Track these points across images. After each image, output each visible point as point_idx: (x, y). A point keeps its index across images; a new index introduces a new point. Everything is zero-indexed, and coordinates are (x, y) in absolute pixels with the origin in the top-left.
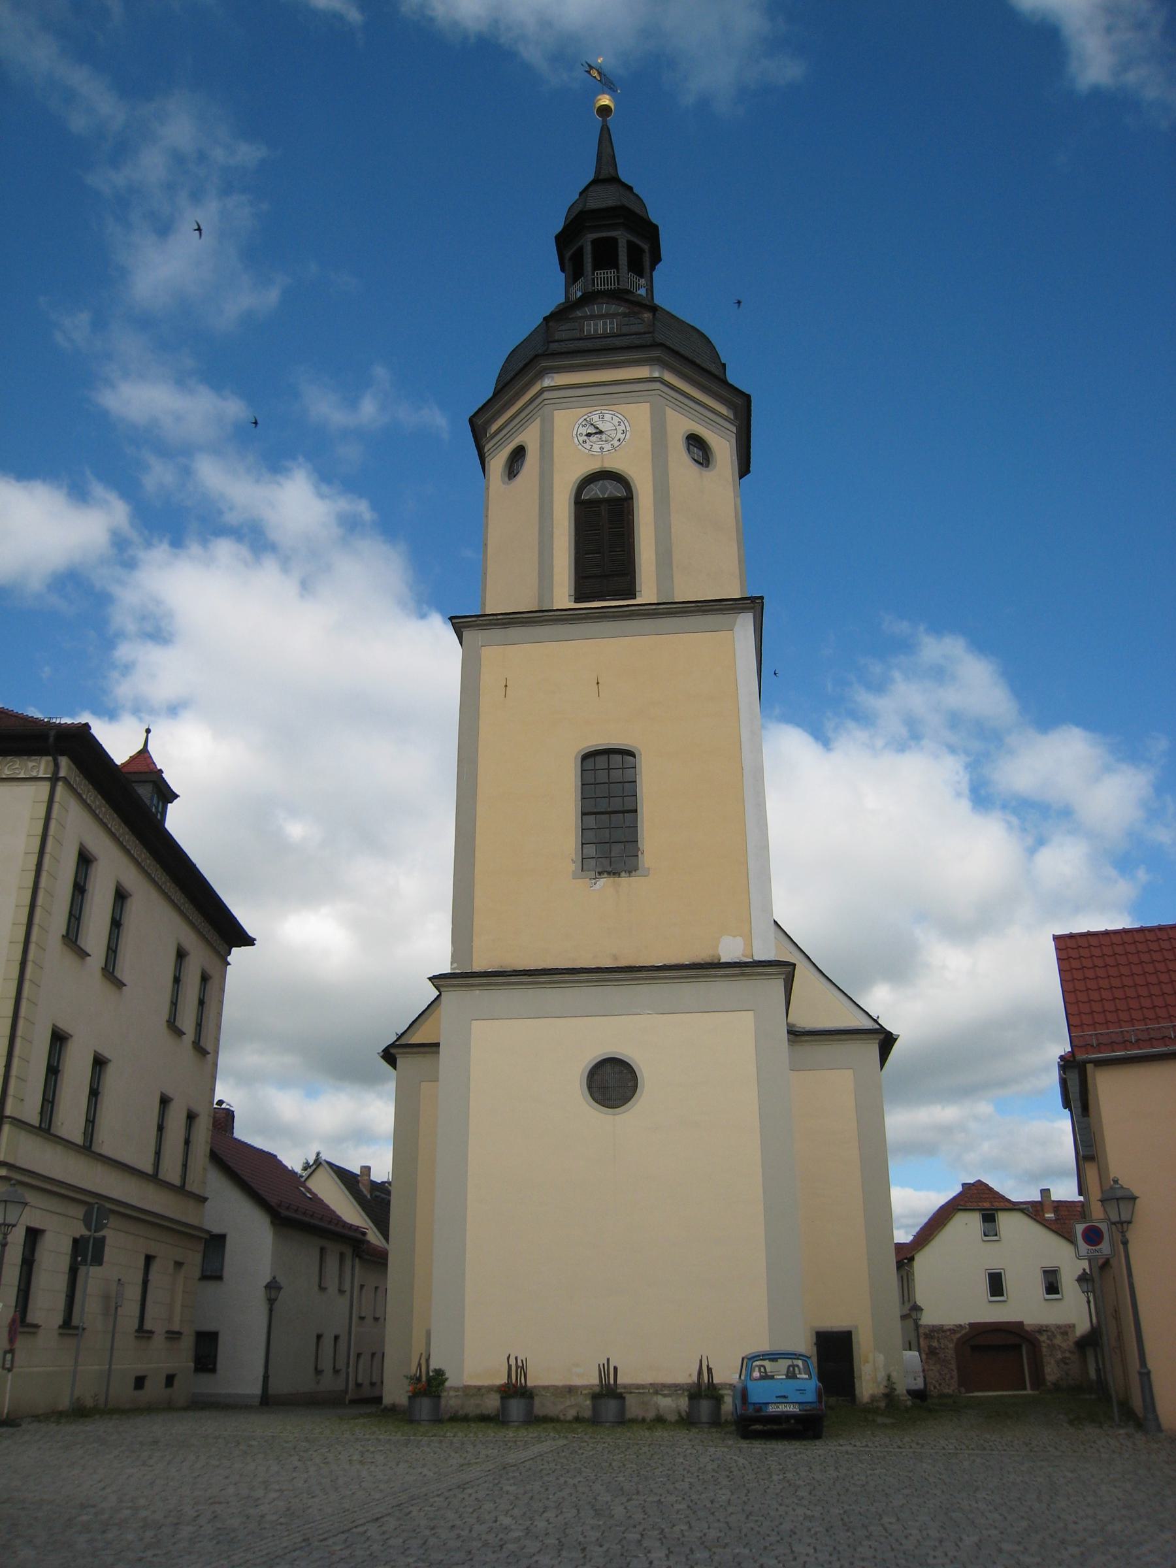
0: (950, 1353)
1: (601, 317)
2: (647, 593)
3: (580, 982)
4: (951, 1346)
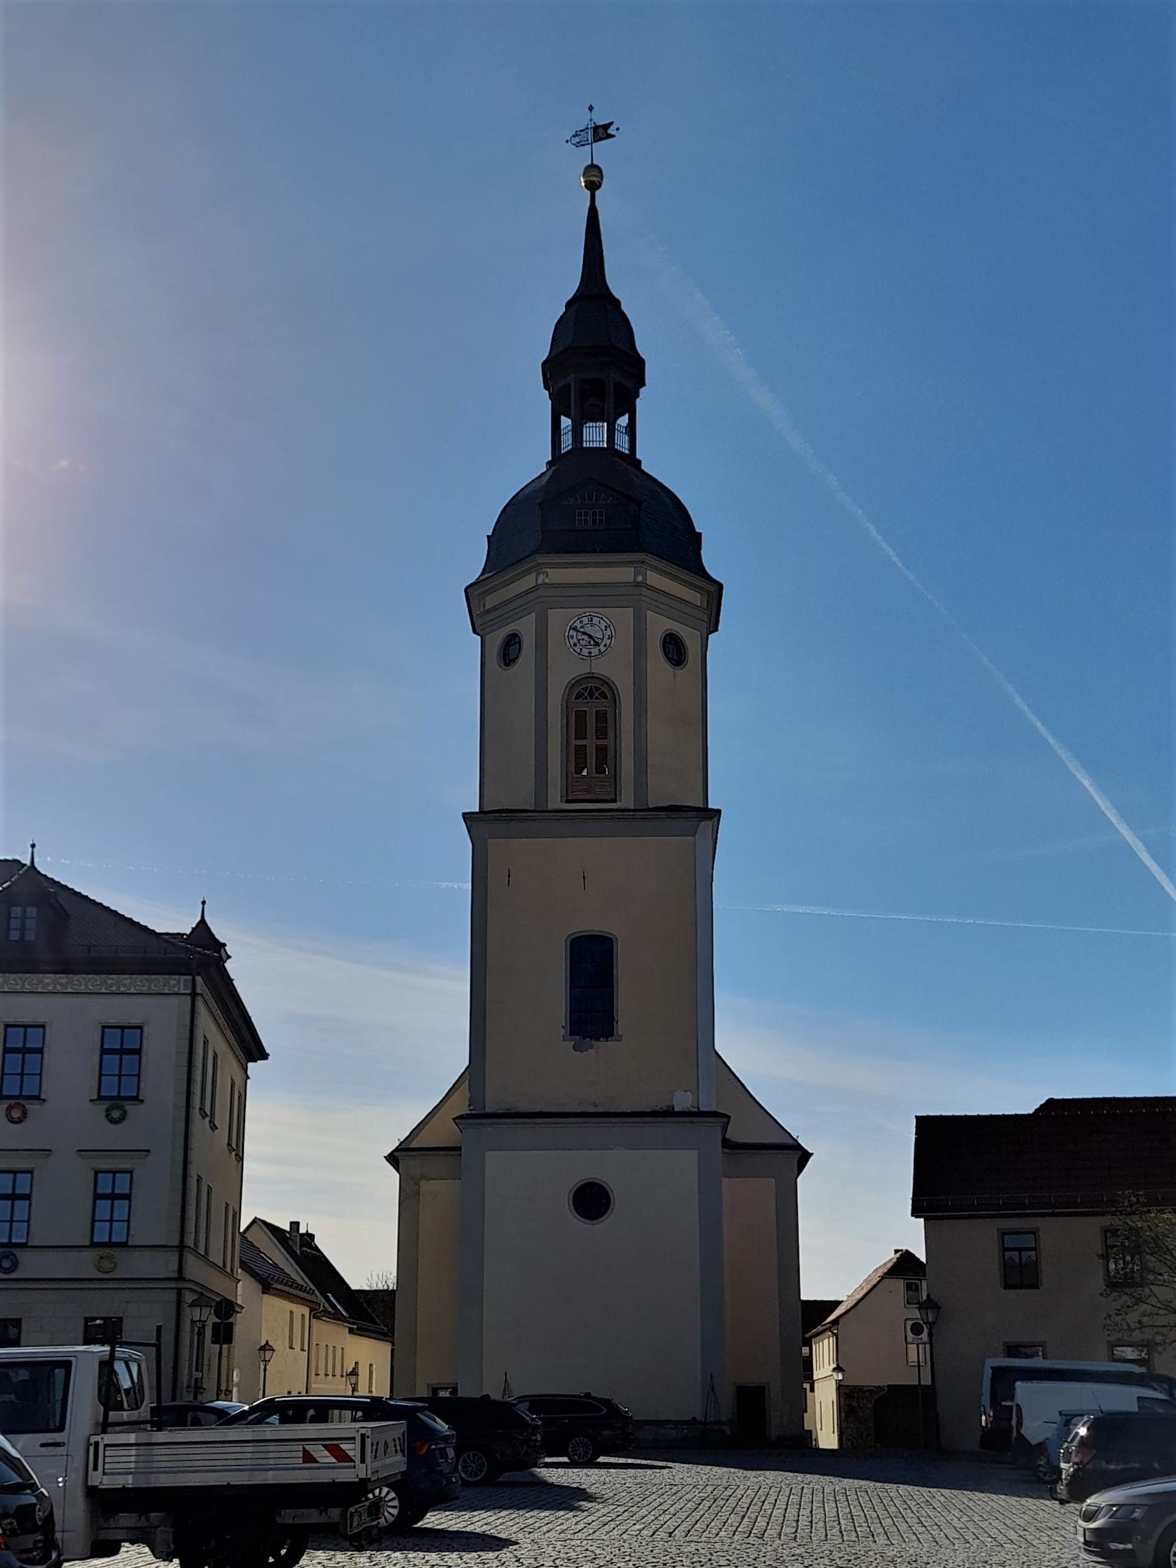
2: (627, 800)
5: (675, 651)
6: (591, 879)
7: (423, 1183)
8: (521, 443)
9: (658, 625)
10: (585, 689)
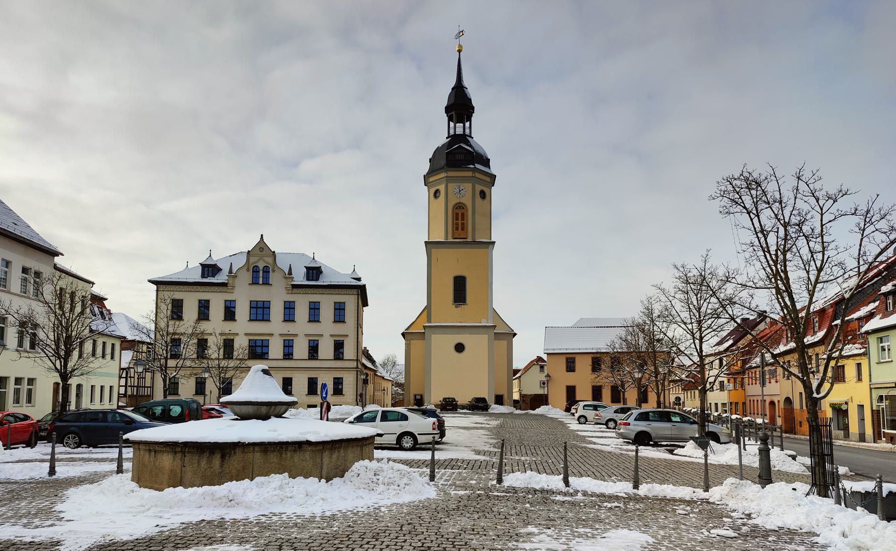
5: (483, 195)
6: (456, 261)
8: (439, 132)
9: (479, 188)
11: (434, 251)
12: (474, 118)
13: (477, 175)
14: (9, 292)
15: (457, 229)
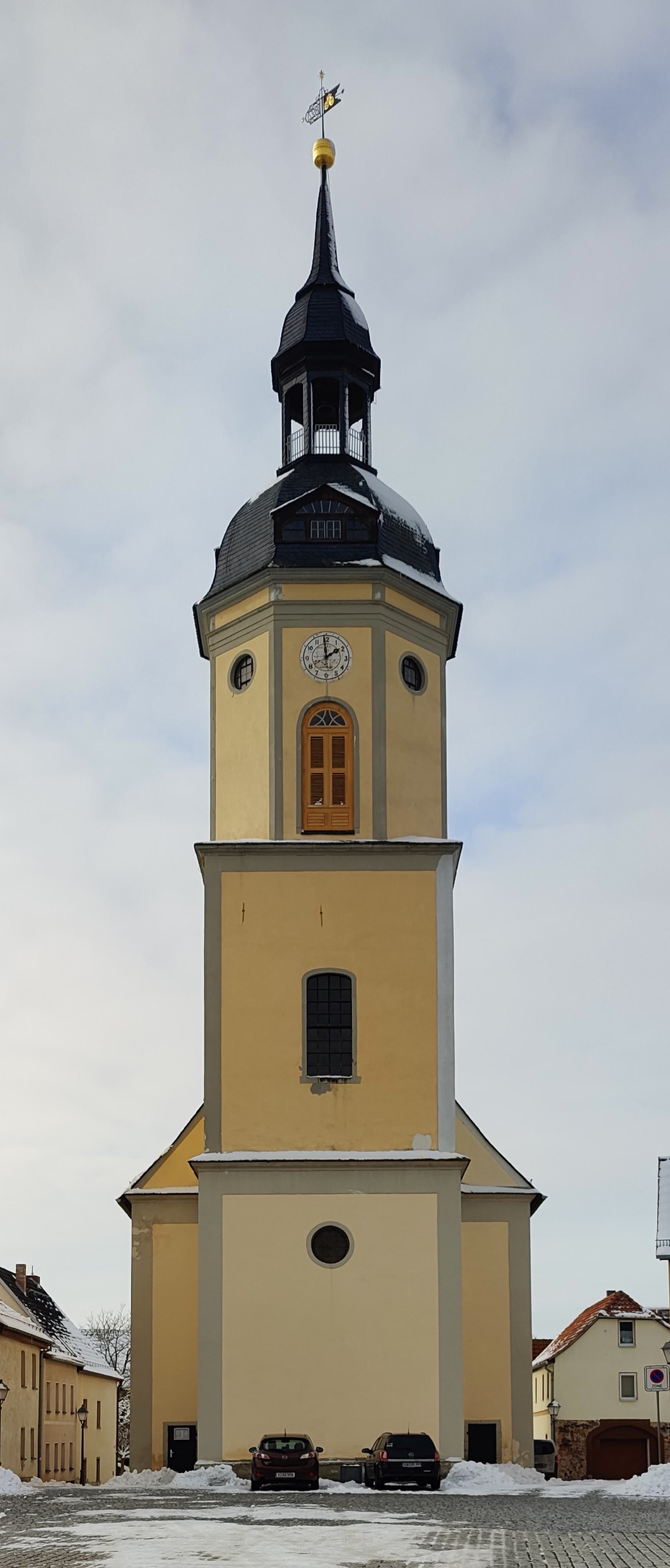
0: (582, 1445)
1: (326, 517)
3: (308, 1167)
4: (583, 1439)
5: (414, 674)
6: (324, 917)
7: (156, 1227)
8: (248, 452)
9: (398, 647)
10: (321, 714)
11: (230, 880)
12: (380, 406)
13: (393, 598)
14: (118, 1401)
15: (317, 795)
